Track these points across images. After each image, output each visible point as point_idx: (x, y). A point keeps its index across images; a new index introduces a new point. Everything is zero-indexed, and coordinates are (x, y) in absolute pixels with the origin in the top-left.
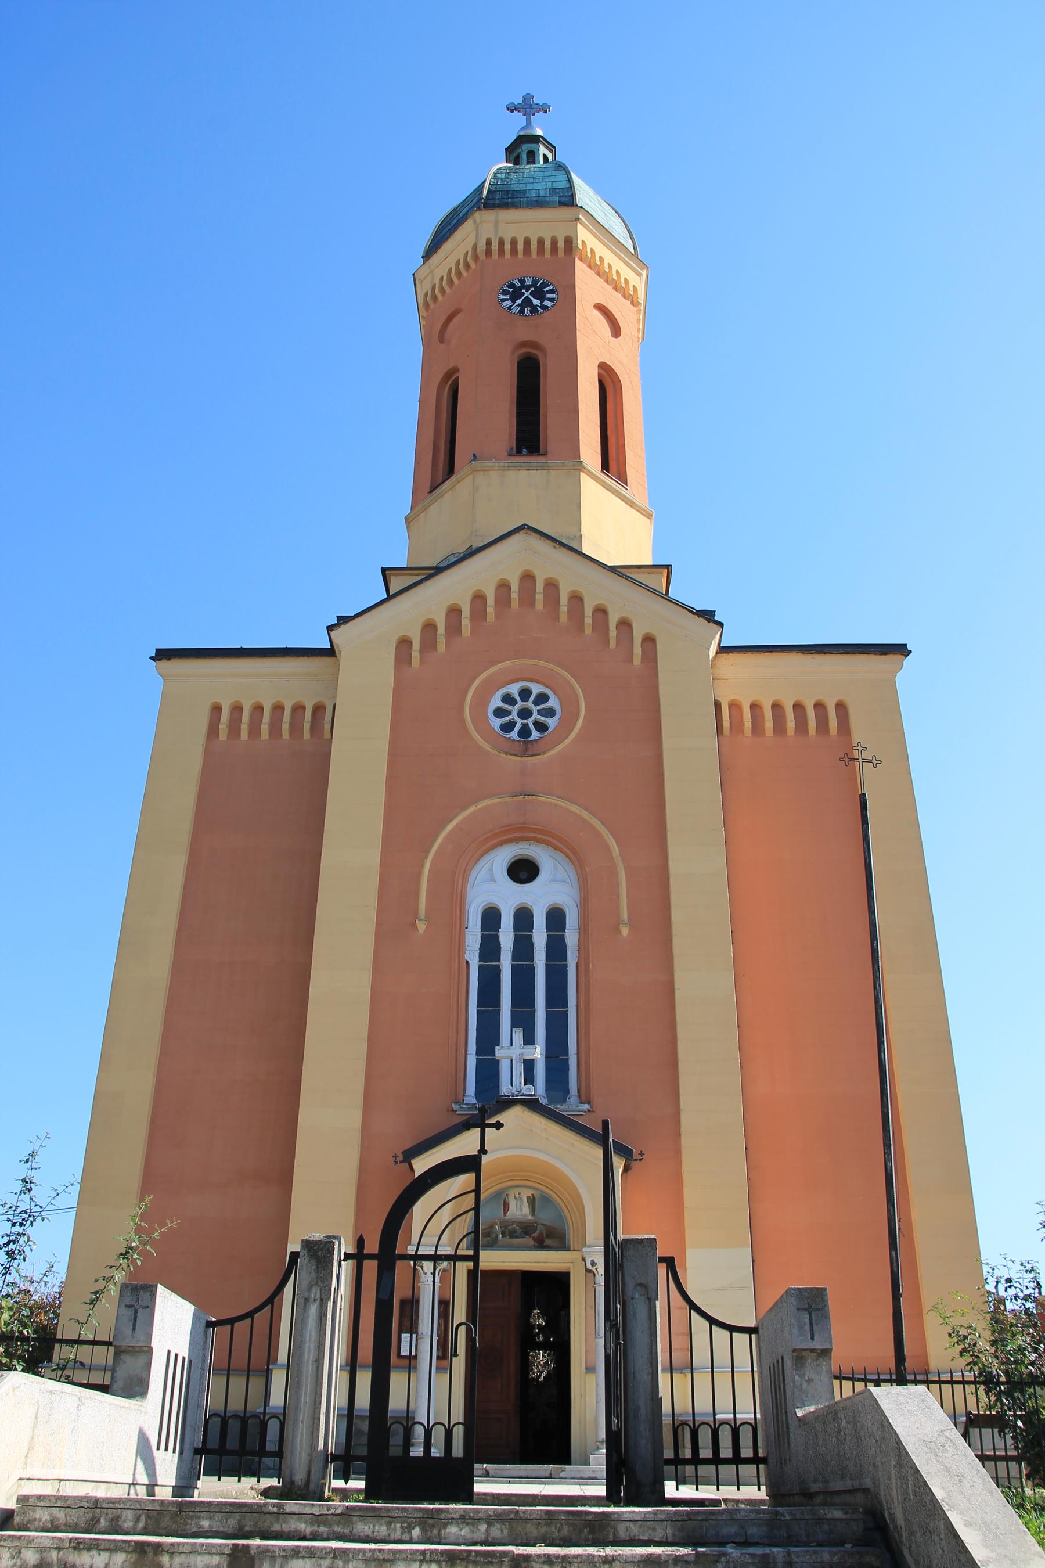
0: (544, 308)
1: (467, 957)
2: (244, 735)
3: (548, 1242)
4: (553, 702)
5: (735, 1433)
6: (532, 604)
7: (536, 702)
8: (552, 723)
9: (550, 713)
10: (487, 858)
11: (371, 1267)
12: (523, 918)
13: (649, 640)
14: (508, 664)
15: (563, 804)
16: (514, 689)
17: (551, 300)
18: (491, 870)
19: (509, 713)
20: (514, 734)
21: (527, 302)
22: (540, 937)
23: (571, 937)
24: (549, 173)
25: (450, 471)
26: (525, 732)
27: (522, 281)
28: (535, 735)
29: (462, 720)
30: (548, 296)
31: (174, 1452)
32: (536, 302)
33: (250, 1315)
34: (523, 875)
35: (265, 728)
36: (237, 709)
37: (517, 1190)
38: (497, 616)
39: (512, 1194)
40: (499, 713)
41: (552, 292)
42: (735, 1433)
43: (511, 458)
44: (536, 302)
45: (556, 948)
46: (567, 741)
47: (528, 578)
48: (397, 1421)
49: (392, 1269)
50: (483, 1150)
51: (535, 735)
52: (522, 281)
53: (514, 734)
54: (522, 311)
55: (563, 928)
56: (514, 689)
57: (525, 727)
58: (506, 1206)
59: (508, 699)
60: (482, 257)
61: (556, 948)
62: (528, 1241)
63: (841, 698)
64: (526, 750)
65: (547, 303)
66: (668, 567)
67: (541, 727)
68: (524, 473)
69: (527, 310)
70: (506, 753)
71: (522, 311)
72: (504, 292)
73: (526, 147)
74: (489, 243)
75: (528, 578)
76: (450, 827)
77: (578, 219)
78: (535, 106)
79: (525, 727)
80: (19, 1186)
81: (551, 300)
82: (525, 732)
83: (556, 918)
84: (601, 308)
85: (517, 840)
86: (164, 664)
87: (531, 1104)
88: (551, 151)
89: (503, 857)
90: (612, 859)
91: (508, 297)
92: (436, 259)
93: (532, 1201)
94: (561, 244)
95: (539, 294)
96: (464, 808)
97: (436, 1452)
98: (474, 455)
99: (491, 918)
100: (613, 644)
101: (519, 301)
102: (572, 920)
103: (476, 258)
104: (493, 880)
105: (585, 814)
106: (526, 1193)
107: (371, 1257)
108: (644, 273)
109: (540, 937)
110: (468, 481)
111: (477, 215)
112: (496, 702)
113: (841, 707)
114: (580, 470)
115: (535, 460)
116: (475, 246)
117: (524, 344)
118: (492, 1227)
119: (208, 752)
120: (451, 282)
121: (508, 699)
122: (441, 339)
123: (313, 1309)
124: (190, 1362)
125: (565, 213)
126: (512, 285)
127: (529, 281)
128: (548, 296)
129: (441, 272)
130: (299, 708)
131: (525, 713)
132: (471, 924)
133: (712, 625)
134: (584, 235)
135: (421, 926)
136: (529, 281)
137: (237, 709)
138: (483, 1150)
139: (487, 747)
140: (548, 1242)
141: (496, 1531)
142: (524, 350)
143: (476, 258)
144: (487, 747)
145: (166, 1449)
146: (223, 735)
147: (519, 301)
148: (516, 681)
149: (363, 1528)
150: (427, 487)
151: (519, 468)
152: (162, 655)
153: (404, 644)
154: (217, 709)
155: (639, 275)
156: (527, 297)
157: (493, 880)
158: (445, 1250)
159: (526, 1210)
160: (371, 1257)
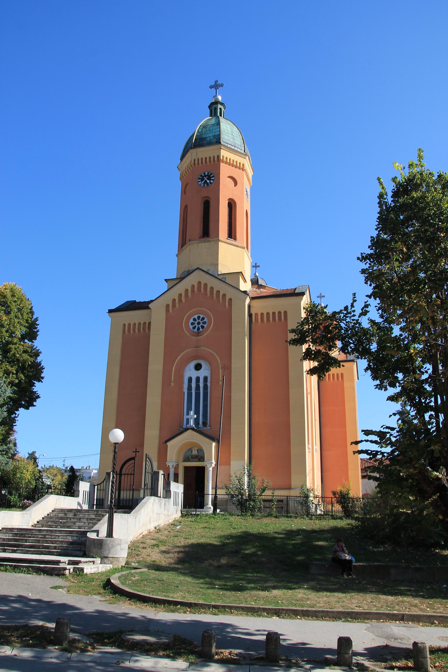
0: (211, 183)
1: (184, 391)
2: (132, 332)
3: (201, 460)
4: (202, 316)
5: (123, 501)
6: (201, 291)
7: (202, 320)
8: (205, 326)
9: (203, 319)
10: (190, 363)
11: (118, 476)
12: (198, 379)
13: (230, 299)
14: (194, 309)
15: (207, 349)
16: (196, 317)
17: (213, 180)
18: (190, 367)
19: (195, 324)
20: (196, 330)
21: (206, 181)
22: (201, 385)
23: (209, 384)
24: (214, 128)
25: (185, 244)
26: (198, 329)
27: (204, 174)
28: (201, 329)
29: (183, 327)
30: (212, 178)
31: (232, 205)
32: (208, 181)
33: (100, 484)
34: (199, 368)
35: (136, 330)
36: (130, 325)
37: (194, 448)
38: (192, 295)
39: (193, 449)
40: (192, 324)
41: (213, 177)
42: (123, 501)
43: (200, 239)
44: (208, 181)
45: (205, 387)
46: (208, 332)
47: (199, 283)
48: (122, 500)
49: (121, 476)
50: (136, 456)
51: (201, 329)
52: (204, 174)
53: (196, 330)
54: (204, 185)
55: (199, 382)
56: (196, 317)
57: (199, 327)
58: (192, 452)
59: (194, 320)
60: (193, 166)
61: (205, 387)
62: (197, 460)
63: (286, 310)
64: (198, 334)
65: (212, 181)
66: (241, 272)
67: (203, 327)
68: (203, 244)
69: (206, 185)
70: (193, 336)
71: (204, 185)
72: (199, 179)
73: (214, 106)
74: (195, 160)
75: (199, 283)
76: (179, 357)
77: (221, 148)
78: (218, 85)
79: (199, 327)
80: (63, 465)
81: (213, 180)
82: (198, 329)
83: (206, 379)
84: (231, 177)
85: (196, 359)
86: (110, 314)
87: (193, 429)
88: (223, 105)
89: (192, 365)
90: (218, 363)
91: (200, 180)
92: (185, 159)
93: (198, 450)
94: (216, 159)
95: (209, 179)
96: (183, 351)
97: (128, 504)
98: (189, 240)
99: (190, 379)
100: (221, 302)
101: (203, 182)
102: (209, 380)
103: (191, 166)
104: (190, 370)
105: (212, 352)
106: (196, 448)
107: (118, 474)
108: (247, 158)
109: (201, 385)
110: (189, 247)
111: (191, 151)
112: (191, 321)
113: (285, 312)
114: (219, 241)
115: (208, 239)
116: (191, 161)
117: (205, 197)
118: (189, 456)
119: (123, 337)
120: (186, 173)
121: (194, 320)
122: (185, 193)
123: (108, 483)
124: (90, 492)
125: (216, 147)
126: (202, 176)
127: (206, 173)
128: (212, 178)
129: (187, 163)
130: (145, 323)
131: (199, 323)
132: (185, 382)
133: (246, 295)
134: (224, 153)
135: (172, 384)
136: (206, 173)
137: (130, 325)
138: (136, 456)
139: (188, 334)
140: (201, 460)
141: (104, 512)
142: (205, 199)
143: (191, 166)
144: (188, 334)
145: (85, 504)
146: (127, 333)
147: (203, 182)
148: (196, 314)
149: (90, 512)
150: (181, 246)
151: (202, 242)
152: (110, 311)
153: (168, 306)
154: (125, 325)
155: (245, 158)
156: (206, 180)
157: (190, 370)
158: (130, 473)
159: (196, 452)
160: (118, 474)
